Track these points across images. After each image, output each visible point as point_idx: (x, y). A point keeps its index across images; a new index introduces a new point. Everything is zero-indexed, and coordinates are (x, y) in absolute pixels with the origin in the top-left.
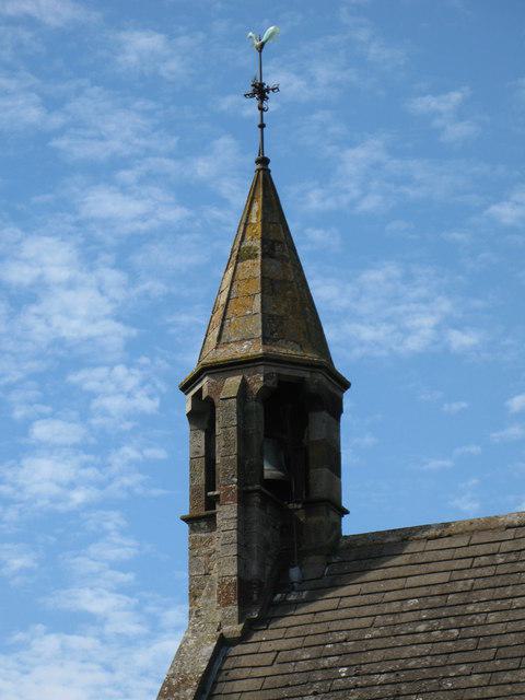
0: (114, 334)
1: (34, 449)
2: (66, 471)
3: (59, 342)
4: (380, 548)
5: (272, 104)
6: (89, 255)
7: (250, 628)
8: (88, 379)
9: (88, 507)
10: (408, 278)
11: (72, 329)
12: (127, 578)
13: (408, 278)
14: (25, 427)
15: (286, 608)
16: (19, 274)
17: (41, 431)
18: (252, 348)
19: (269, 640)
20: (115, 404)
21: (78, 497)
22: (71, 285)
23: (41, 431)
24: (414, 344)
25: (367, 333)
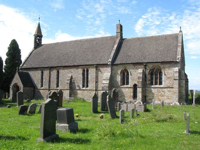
0: (102, 11)
1: (97, 20)
2: (99, 22)
3: (98, 12)
4: (43, 45)
5: (39, 17)
6: (101, 5)
7: (35, 50)
8: (101, 15)
9: (101, 25)
10: (125, 8)
11: (100, 11)
12: (104, 30)
13: (125, 8)
14: (96, 19)
15: (37, 48)
16: (95, 7)
17: (97, 19)
18: (36, 34)
19: (35, 50)
20: (103, 17)
21: (100, 24)
22: (99, 8)
23: (97, 19)
24: (126, 13)
25: (122, 12)
